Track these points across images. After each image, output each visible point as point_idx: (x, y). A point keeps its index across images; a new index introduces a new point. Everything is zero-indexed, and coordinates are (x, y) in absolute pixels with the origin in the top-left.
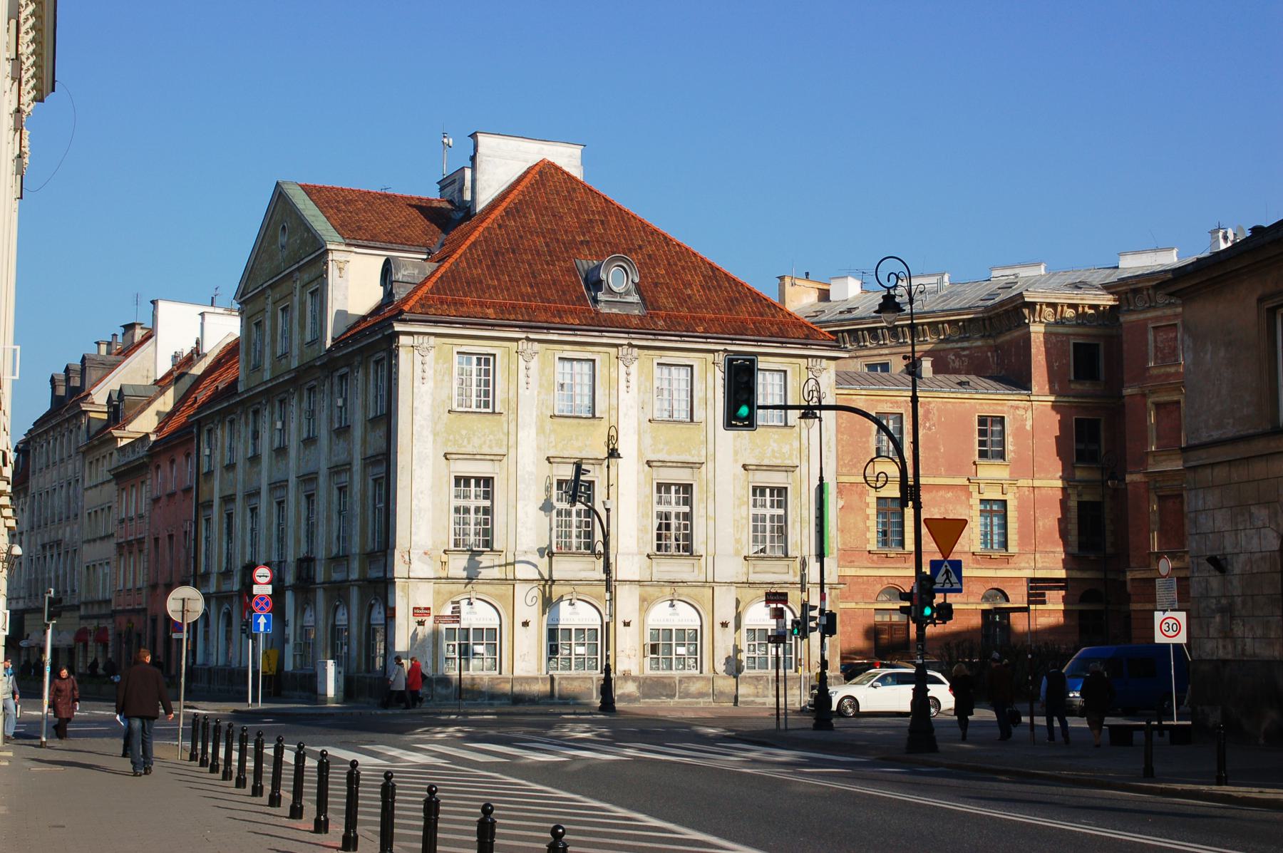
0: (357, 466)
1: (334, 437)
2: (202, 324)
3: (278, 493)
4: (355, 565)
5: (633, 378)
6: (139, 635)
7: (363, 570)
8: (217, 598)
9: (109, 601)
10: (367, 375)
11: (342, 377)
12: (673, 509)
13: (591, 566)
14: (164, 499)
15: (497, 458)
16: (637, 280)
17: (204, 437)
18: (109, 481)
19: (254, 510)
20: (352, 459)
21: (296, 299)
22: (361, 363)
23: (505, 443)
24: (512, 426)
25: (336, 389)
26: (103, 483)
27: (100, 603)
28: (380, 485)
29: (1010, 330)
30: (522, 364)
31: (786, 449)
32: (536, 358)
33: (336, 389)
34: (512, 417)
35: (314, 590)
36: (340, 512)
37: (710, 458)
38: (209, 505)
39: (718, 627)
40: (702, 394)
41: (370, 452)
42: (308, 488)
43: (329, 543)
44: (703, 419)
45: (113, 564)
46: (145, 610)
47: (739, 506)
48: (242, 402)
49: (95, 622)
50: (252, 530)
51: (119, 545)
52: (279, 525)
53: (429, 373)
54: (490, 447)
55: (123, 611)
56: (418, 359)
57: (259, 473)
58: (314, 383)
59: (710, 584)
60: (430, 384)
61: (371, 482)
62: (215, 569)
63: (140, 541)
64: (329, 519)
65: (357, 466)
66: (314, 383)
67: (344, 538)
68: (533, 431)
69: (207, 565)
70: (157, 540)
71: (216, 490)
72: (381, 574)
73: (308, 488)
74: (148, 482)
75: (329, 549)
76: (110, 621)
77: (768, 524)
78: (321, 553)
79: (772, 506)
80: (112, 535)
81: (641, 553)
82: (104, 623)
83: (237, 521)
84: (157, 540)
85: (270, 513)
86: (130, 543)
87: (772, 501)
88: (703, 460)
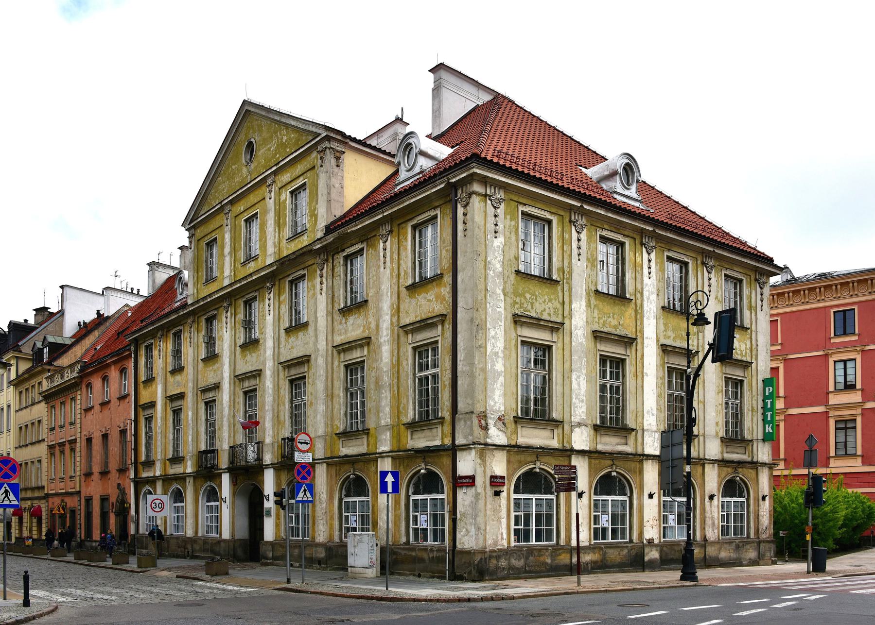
0: (226, 386)
2: (62, 294)
7: (397, 437)
8: (164, 480)
9: (43, 487)
10: (435, 230)
13: (623, 441)
14: (97, 408)
15: (556, 327)
17: (142, 352)
23: (560, 312)
24: (566, 294)
27: (33, 489)
30: (574, 235)
35: (220, 475)
38: (152, 405)
39: (707, 499)
45: (45, 461)
46: (79, 493)
49: (29, 503)
51: (51, 447)
53: (501, 227)
54: (549, 315)
55: (57, 495)
56: (491, 210)
60: (499, 242)
65: (226, 386)
68: (584, 303)
76: (44, 501)
80: (43, 440)
82: (36, 503)
85: (165, 419)
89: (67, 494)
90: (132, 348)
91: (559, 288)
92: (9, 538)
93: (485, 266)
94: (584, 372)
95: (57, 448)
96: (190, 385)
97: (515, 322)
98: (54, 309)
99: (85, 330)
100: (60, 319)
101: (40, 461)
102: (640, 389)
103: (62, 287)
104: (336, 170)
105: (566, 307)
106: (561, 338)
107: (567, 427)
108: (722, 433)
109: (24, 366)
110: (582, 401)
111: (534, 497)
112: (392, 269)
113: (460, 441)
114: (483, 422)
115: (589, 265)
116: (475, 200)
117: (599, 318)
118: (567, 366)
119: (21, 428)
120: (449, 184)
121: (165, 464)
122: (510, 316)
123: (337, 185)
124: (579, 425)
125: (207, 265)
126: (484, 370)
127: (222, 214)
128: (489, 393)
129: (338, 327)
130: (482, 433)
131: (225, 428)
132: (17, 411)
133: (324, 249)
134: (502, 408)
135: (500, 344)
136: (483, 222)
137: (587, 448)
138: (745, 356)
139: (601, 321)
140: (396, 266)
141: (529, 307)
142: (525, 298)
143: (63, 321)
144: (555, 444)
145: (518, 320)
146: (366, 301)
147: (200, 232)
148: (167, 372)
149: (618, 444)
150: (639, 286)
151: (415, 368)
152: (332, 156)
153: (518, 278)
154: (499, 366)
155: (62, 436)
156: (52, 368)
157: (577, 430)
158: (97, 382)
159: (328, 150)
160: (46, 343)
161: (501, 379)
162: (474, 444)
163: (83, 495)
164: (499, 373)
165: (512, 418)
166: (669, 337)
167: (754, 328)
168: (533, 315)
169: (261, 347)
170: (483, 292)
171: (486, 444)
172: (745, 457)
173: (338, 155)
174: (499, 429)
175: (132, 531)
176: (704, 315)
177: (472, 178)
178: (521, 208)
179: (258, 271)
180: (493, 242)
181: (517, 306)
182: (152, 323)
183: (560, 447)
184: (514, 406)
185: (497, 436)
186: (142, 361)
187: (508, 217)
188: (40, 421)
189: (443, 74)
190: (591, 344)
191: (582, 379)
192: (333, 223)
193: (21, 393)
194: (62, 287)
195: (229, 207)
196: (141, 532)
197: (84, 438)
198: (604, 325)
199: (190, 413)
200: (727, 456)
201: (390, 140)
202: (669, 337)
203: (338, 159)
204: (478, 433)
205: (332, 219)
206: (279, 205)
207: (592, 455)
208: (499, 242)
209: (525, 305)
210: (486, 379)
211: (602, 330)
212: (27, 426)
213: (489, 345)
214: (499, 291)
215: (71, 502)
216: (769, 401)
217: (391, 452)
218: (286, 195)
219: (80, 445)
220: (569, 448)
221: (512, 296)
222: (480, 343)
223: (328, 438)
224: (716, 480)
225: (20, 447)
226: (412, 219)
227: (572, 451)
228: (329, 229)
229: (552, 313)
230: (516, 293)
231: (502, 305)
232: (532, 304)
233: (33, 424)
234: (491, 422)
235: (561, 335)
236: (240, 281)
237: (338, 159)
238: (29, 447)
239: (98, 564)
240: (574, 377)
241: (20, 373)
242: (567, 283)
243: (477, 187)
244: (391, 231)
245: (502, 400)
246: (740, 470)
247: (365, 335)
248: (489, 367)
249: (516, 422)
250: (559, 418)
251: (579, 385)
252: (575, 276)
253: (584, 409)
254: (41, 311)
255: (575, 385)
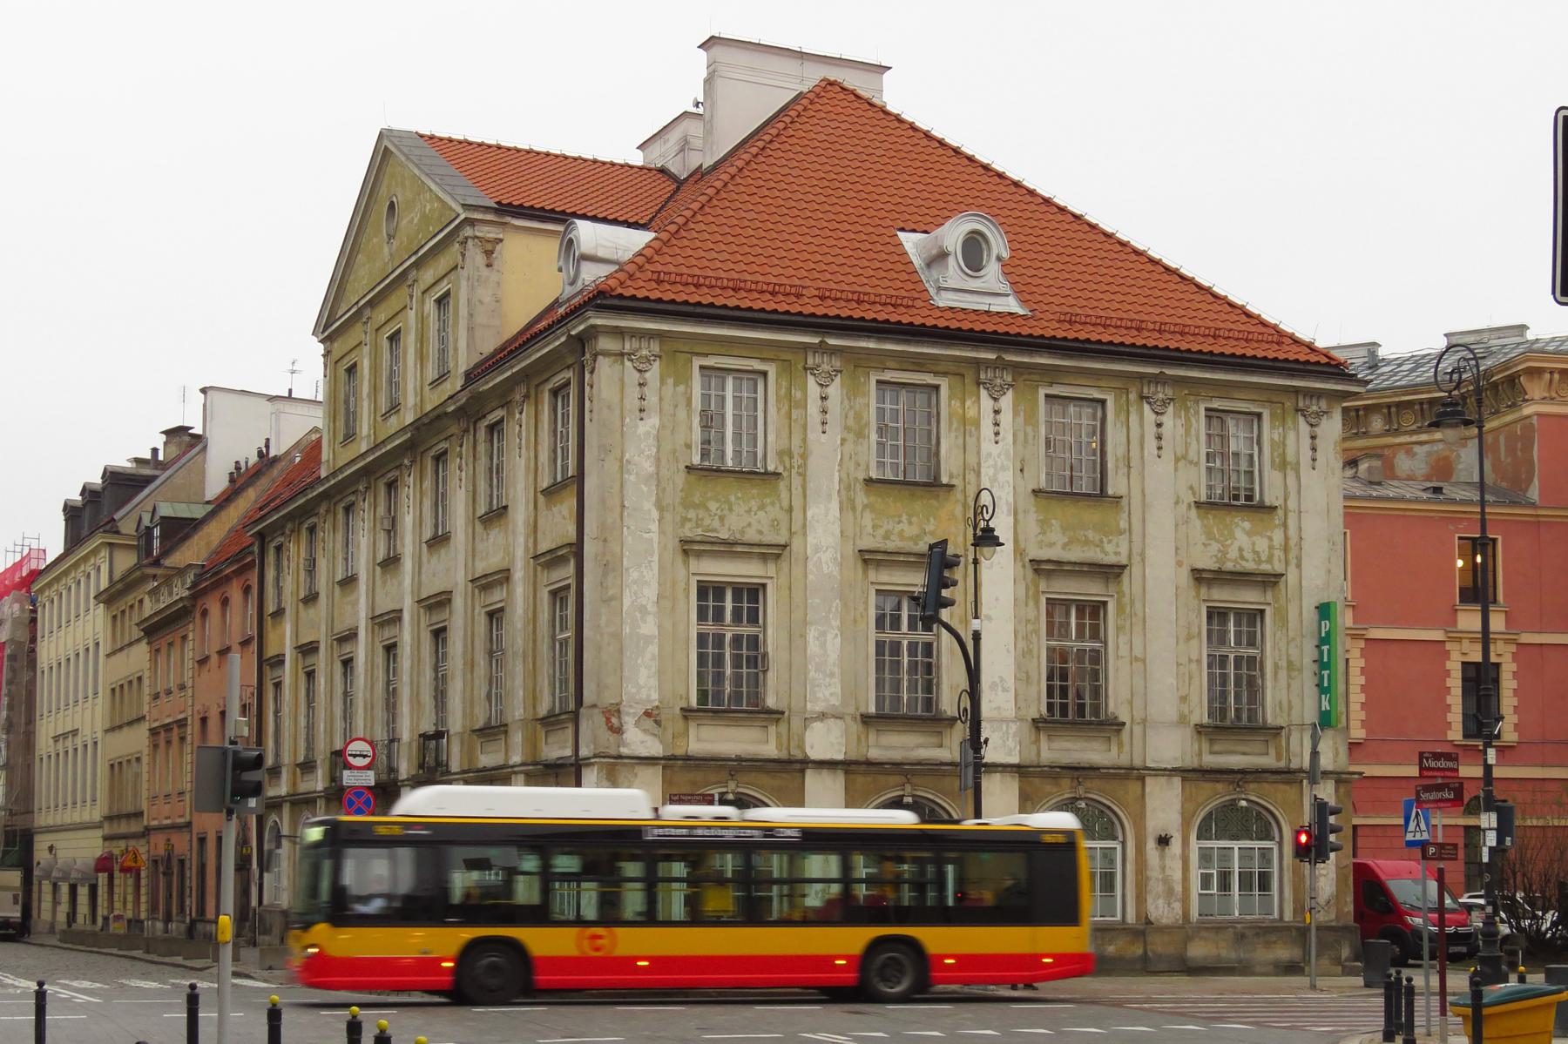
1: (479, 527)
3: (388, 633)
4: (517, 738)
5: (1006, 418)
6: (182, 862)
7: (532, 744)
8: (294, 803)
11: (491, 428)
12: (1073, 644)
14: (214, 658)
15: (774, 553)
16: (1006, 254)
17: (271, 557)
18: (138, 640)
19: (347, 663)
20: (513, 561)
21: (412, 314)
22: (527, 397)
25: (482, 448)
26: (130, 644)
27: (129, 816)
28: (564, 601)
29: (1497, 412)
31: (1262, 544)
32: (838, 380)
33: (482, 448)
34: (796, 482)
36: (491, 653)
37: (1136, 559)
38: (279, 661)
39: (1151, 845)
40: (1121, 451)
41: (544, 547)
42: (435, 618)
43: (469, 702)
44: (1122, 491)
45: (145, 760)
46: (189, 825)
47: (1189, 638)
48: (325, 496)
49: (122, 844)
50: (346, 693)
51: (154, 732)
52: (388, 683)
53: (652, 399)
57: (355, 603)
58: (444, 445)
59: (1136, 774)
60: (652, 422)
61: (544, 595)
62: (286, 758)
63: (182, 723)
64: (471, 665)
66: (444, 445)
67: (495, 691)
68: (835, 505)
69: (277, 755)
70: (204, 720)
71: (284, 639)
72: (568, 752)
73: (435, 618)
74: (191, 636)
75: (468, 713)
76: (143, 841)
77: (1231, 669)
78: (456, 723)
79: (1238, 643)
81: (1019, 719)
83: (321, 681)
84: (204, 720)
86: (167, 728)
87: (1238, 634)
88: (1124, 562)
89: (174, 827)
90: (256, 549)
91: (782, 485)
92: (94, 921)
93: (621, 467)
94: (836, 623)
95: (176, 730)
96: (323, 628)
97: (685, 552)
98: (198, 430)
99: (241, 480)
100: (199, 458)
101: (138, 759)
102: (1022, 635)
103: (204, 391)
104: (485, 272)
105: (797, 514)
106: (786, 570)
107: (796, 723)
108: (1201, 715)
109: (126, 561)
110: (832, 675)
111: (1236, 845)
112: (528, 459)
113: (584, 752)
114: (614, 720)
115: (851, 437)
116: (603, 364)
117: (875, 527)
118: (797, 615)
119: (113, 690)
120: (570, 336)
121: (294, 774)
122: (673, 544)
123: (487, 299)
124: (823, 716)
125: (347, 409)
126: (617, 636)
127: (359, 325)
128: (626, 673)
129: (480, 546)
130: (612, 738)
131: (361, 711)
132: (108, 656)
133: (461, 412)
134: (655, 696)
135: (650, 593)
136: (616, 399)
137: (841, 757)
138: (1270, 560)
139: (881, 532)
140: (532, 454)
141: (716, 524)
142: (708, 509)
143: (204, 461)
144: (770, 750)
145: (688, 549)
146: (505, 508)
147: (339, 347)
148: (357, 578)
149: (918, 746)
150: (971, 460)
151: (554, 626)
152: (479, 251)
153: (692, 478)
154: (649, 627)
155: (166, 713)
156: (159, 572)
157: (817, 725)
158: (214, 608)
159: (470, 242)
160: (157, 518)
161: (653, 649)
162: (595, 756)
163: (195, 831)
164: (648, 640)
165: (678, 711)
166: (1051, 545)
167: (1292, 504)
168: (724, 535)
169: (397, 568)
170: (618, 509)
171: (620, 757)
172: (1268, 761)
173: (489, 247)
174: (645, 731)
175: (254, 902)
176: (993, 530)
177: (593, 332)
178: (697, 362)
179: (353, 461)
180: (636, 426)
181: (688, 525)
182: (276, 509)
183: (784, 755)
184: (683, 692)
185: (639, 741)
186: (270, 574)
187: (670, 381)
188: (140, 679)
189: (717, 51)
190: (855, 571)
191: (829, 637)
192: (476, 366)
193: (114, 617)
194: (204, 391)
195: (367, 312)
196: (265, 902)
197: (197, 718)
198: (886, 537)
199: (322, 681)
200: (1210, 761)
201: (677, 148)
202: (1051, 545)
203: (488, 253)
204: (607, 741)
205: (477, 359)
206: (422, 319)
207: (853, 767)
208: (652, 422)
209: (707, 522)
210: (621, 651)
211: (883, 547)
212: (130, 682)
213: (627, 593)
214: (649, 506)
215: (182, 844)
216: (1325, 648)
217: (523, 764)
218: (430, 306)
219: (192, 730)
220: (800, 756)
221: (680, 509)
222: (611, 592)
223: (466, 736)
224: (1177, 806)
225: (112, 729)
226: (547, 380)
227: (805, 764)
228: (471, 377)
229: (765, 530)
230: (687, 504)
231: (654, 527)
232: (722, 519)
233: (130, 682)
234: (629, 722)
235: (784, 565)
236: (341, 469)
237: (488, 253)
238: (125, 729)
239: (167, 960)
240: (812, 633)
241: (117, 575)
242: (799, 474)
243: (604, 343)
244: (527, 397)
245: (654, 682)
246: (1252, 786)
247: (504, 565)
248: (627, 630)
249: (685, 718)
250: (781, 706)
251: (823, 645)
252: (813, 462)
253: (837, 689)
254: (175, 434)
255: (813, 647)
